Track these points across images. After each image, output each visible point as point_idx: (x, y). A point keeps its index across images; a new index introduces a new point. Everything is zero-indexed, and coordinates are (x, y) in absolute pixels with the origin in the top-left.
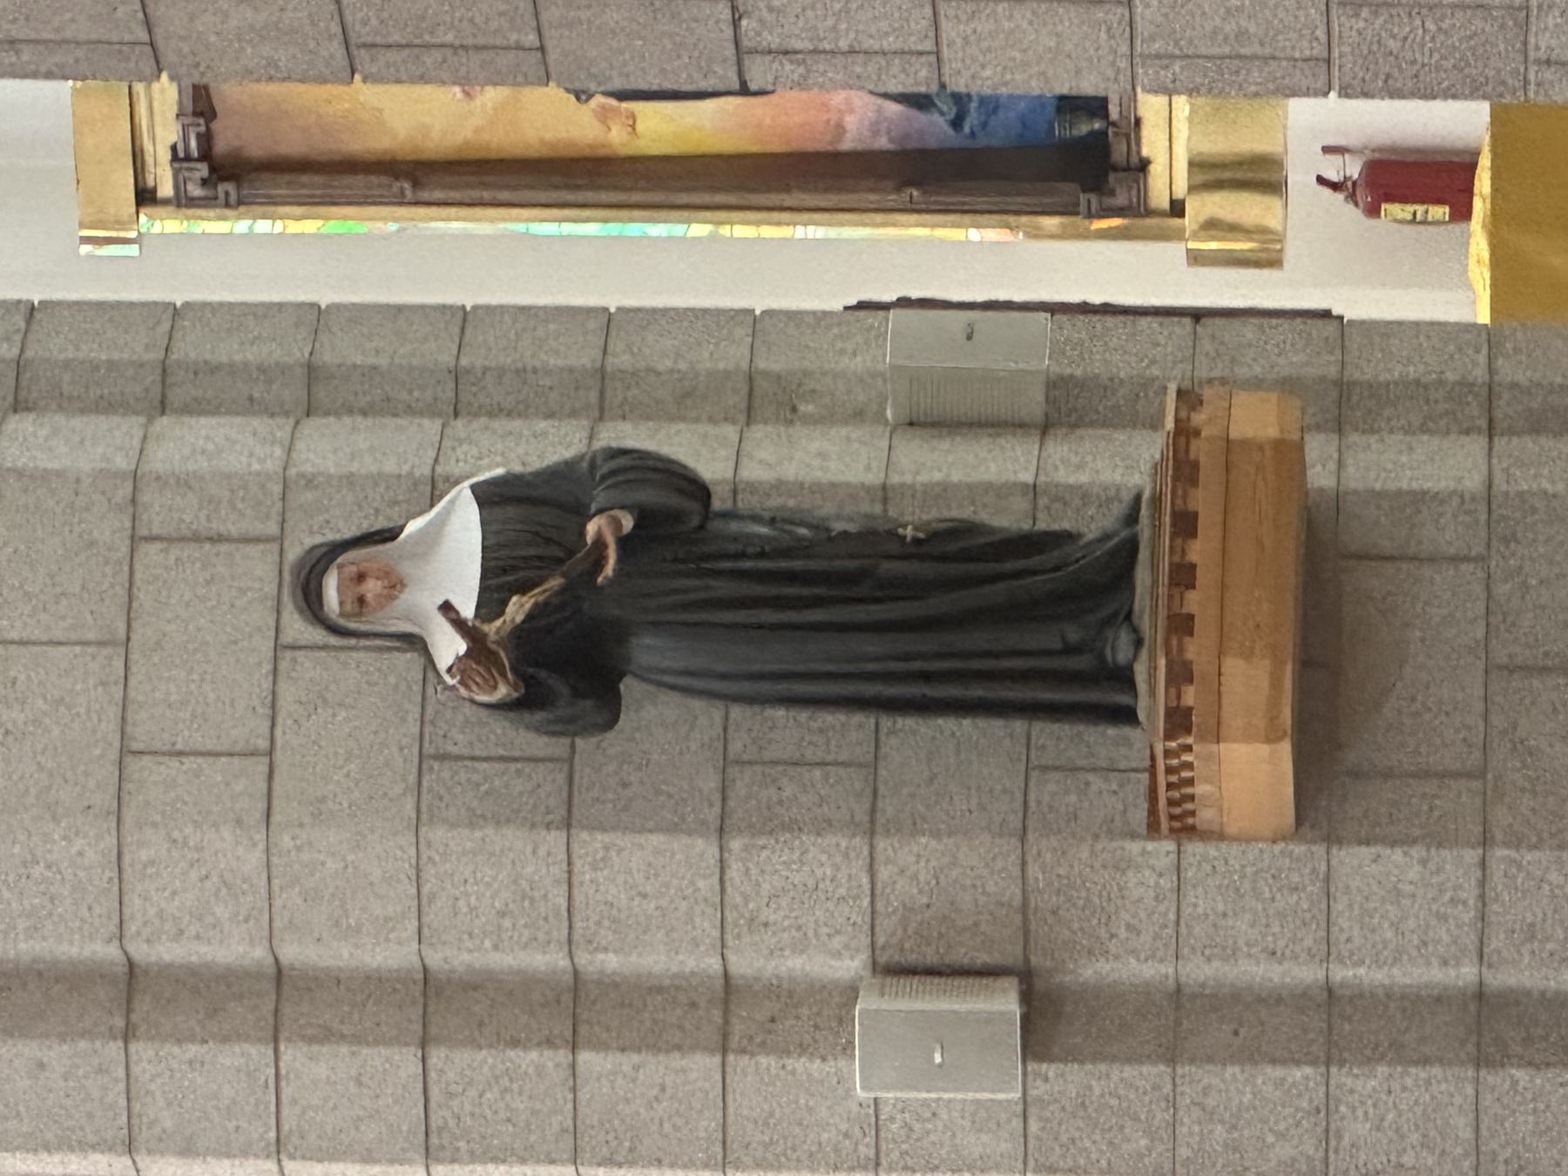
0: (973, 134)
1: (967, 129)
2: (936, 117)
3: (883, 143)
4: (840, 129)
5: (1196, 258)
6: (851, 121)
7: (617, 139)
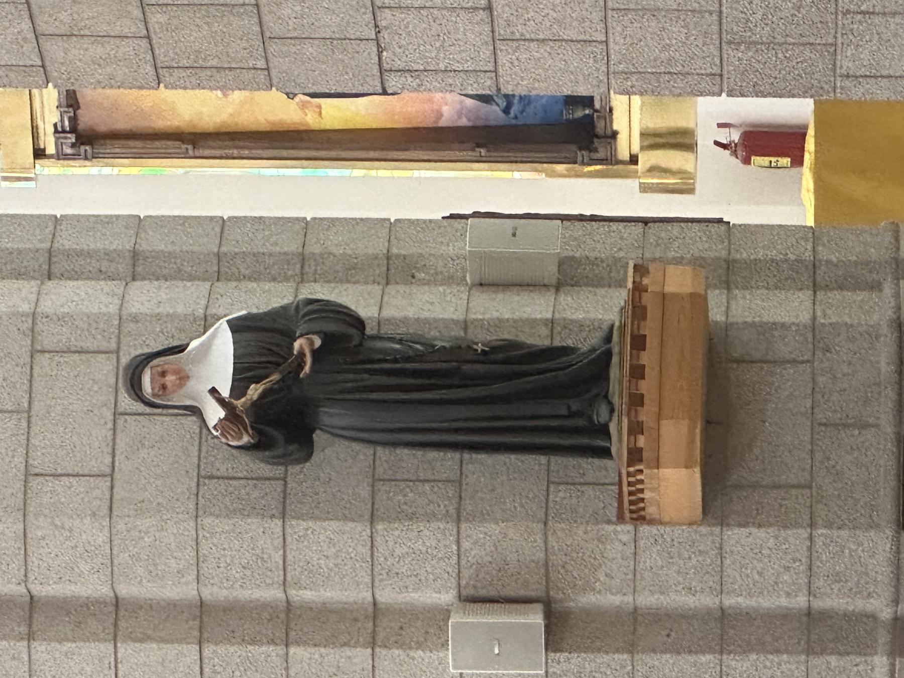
0: (516, 117)
1: (512, 115)
2: (495, 107)
3: (464, 122)
4: (440, 115)
5: (644, 189)
6: (446, 110)
7: (311, 120)
